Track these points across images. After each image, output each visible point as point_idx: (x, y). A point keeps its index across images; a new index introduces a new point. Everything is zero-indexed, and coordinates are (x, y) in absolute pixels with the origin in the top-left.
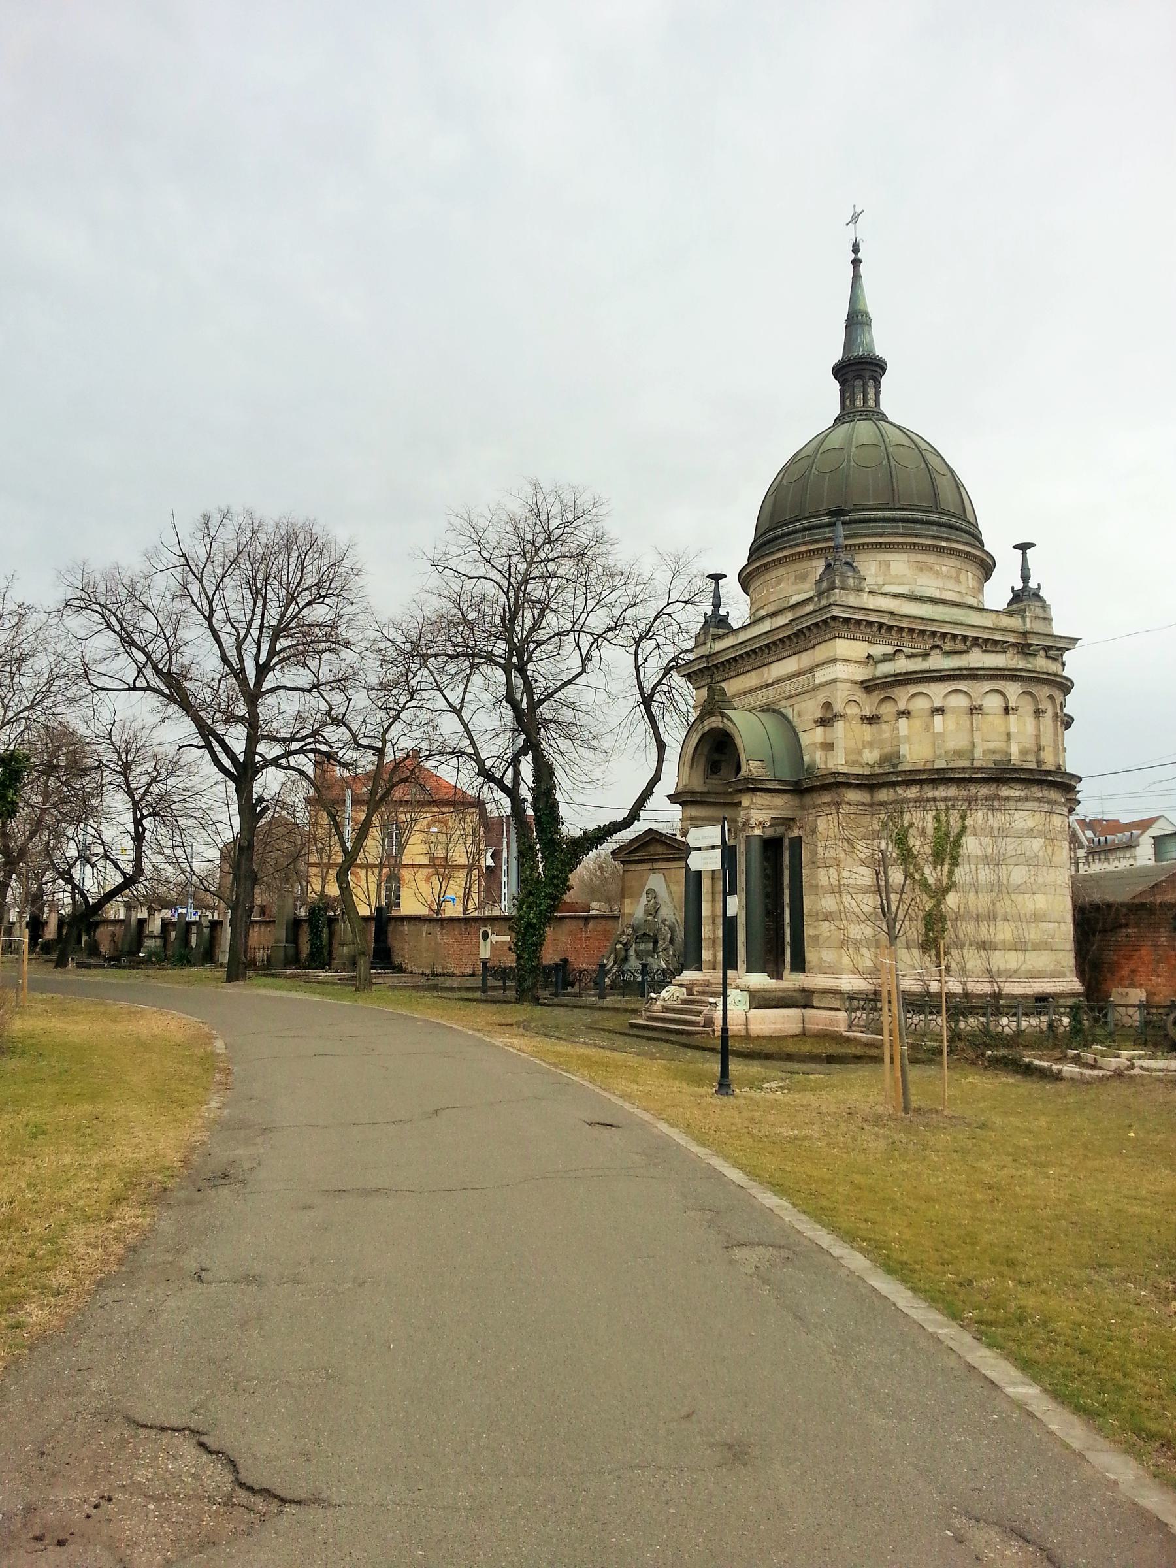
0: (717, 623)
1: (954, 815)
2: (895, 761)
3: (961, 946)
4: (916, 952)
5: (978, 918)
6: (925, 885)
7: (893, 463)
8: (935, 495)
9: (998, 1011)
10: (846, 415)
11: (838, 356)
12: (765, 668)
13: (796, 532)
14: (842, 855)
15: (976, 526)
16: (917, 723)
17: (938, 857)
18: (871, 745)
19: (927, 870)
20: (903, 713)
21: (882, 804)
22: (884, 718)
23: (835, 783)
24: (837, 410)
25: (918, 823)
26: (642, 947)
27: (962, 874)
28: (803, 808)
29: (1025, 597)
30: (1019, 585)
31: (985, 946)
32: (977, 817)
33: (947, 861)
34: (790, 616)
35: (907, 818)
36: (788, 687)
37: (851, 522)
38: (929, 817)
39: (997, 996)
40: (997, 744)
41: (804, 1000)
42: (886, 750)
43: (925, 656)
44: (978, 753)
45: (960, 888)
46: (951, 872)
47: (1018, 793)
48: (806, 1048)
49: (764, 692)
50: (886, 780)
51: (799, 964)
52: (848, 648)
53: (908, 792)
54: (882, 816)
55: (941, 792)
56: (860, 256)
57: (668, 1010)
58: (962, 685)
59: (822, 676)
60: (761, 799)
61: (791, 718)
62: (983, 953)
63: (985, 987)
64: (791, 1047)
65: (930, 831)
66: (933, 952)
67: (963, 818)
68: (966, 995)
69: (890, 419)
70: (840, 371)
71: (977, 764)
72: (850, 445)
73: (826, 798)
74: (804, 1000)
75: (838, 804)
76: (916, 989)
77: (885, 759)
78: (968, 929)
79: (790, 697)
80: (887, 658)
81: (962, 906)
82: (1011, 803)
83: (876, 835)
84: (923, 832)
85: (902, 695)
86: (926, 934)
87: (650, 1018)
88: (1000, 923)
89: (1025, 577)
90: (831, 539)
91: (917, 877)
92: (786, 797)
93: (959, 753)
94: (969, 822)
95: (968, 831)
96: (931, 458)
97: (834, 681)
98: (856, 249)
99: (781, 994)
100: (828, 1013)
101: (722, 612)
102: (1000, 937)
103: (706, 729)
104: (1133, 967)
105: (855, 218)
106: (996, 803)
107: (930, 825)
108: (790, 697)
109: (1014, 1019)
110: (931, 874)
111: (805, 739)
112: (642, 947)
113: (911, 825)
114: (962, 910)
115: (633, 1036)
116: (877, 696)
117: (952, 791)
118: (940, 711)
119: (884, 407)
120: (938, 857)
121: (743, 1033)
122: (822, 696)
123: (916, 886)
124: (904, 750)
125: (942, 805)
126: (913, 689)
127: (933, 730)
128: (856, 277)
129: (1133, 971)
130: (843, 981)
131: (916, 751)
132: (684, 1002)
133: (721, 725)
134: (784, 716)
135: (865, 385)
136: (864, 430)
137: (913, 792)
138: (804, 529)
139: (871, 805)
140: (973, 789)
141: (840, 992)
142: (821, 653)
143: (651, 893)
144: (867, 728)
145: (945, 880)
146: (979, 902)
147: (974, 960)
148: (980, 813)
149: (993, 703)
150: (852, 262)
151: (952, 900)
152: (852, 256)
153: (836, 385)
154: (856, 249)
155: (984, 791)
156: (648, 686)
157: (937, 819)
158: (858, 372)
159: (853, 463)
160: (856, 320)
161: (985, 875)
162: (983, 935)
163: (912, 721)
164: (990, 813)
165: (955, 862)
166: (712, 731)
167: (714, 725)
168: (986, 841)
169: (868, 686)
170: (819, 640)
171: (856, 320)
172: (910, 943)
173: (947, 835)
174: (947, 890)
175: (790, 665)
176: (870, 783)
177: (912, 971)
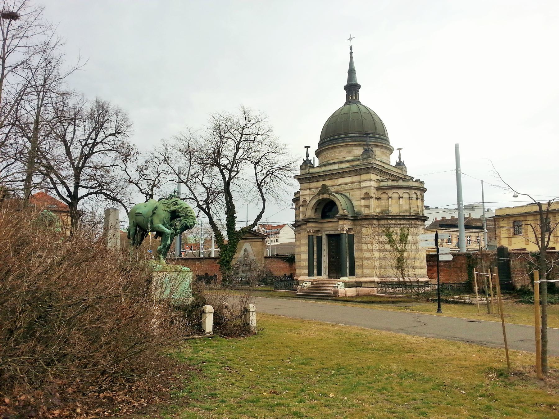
1: (406, 229)
3: (408, 267)
4: (395, 269)
5: (412, 259)
6: (397, 249)
8: (376, 129)
9: (419, 287)
10: (348, 102)
16: (394, 201)
17: (401, 241)
18: (378, 207)
19: (398, 245)
21: (382, 225)
23: (369, 218)
24: (345, 101)
26: (244, 269)
27: (408, 246)
28: (355, 225)
29: (400, 164)
30: (398, 161)
31: (414, 267)
34: (347, 165)
35: (391, 230)
36: (347, 187)
38: (399, 229)
39: (418, 282)
40: (415, 208)
41: (358, 284)
42: (383, 209)
43: (397, 181)
46: (405, 246)
48: (359, 299)
49: (336, 187)
50: (384, 217)
51: (352, 273)
52: (373, 176)
55: (402, 222)
57: (309, 289)
58: (408, 191)
59: (363, 184)
60: (346, 222)
63: (414, 280)
64: (354, 299)
65: (399, 233)
68: (410, 282)
69: (362, 103)
70: (346, 88)
71: (412, 214)
73: (366, 222)
74: (358, 284)
76: (396, 280)
77: (382, 211)
79: (348, 190)
83: (380, 234)
84: (397, 234)
85: (390, 193)
87: (303, 292)
89: (400, 158)
90: (365, 141)
91: (395, 247)
92: (351, 221)
93: (406, 211)
96: (374, 116)
97: (371, 186)
98: (351, 49)
102: (417, 265)
105: (351, 39)
107: (399, 232)
108: (348, 190)
110: (399, 247)
111: (355, 204)
112: (244, 269)
113: (393, 231)
116: (380, 192)
117: (405, 222)
118: (391, 198)
119: (360, 100)
120: (401, 241)
122: (364, 191)
124: (390, 209)
126: (394, 191)
127: (397, 204)
128: (351, 58)
131: (394, 209)
132: (312, 287)
133: (328, 197)
134: (344, 195)
136: (354, 108)
137: (393, 222)
138: (350, 137)
141: (374, 282)
142: (364, 177)
143: (245, 250)
146: (412, 255)
147: (411, 272)
149: (406, 195)
151: (405, 254)
153: (344, 92)
154: (351, 49)
155: (413, 222)
156: (259, 181)
157: (401, 230)
158: (352, 88)
160: (351, 72)
161: (413, 247)
162: (413, 265)
165: (406, 243)
166: (324, 200)
167: (325, 197)
168: (414, 237)
169: (378, 189)
171: (351, 72)
175: (348, 180)
176: (379, 218)
177: (393, 276)
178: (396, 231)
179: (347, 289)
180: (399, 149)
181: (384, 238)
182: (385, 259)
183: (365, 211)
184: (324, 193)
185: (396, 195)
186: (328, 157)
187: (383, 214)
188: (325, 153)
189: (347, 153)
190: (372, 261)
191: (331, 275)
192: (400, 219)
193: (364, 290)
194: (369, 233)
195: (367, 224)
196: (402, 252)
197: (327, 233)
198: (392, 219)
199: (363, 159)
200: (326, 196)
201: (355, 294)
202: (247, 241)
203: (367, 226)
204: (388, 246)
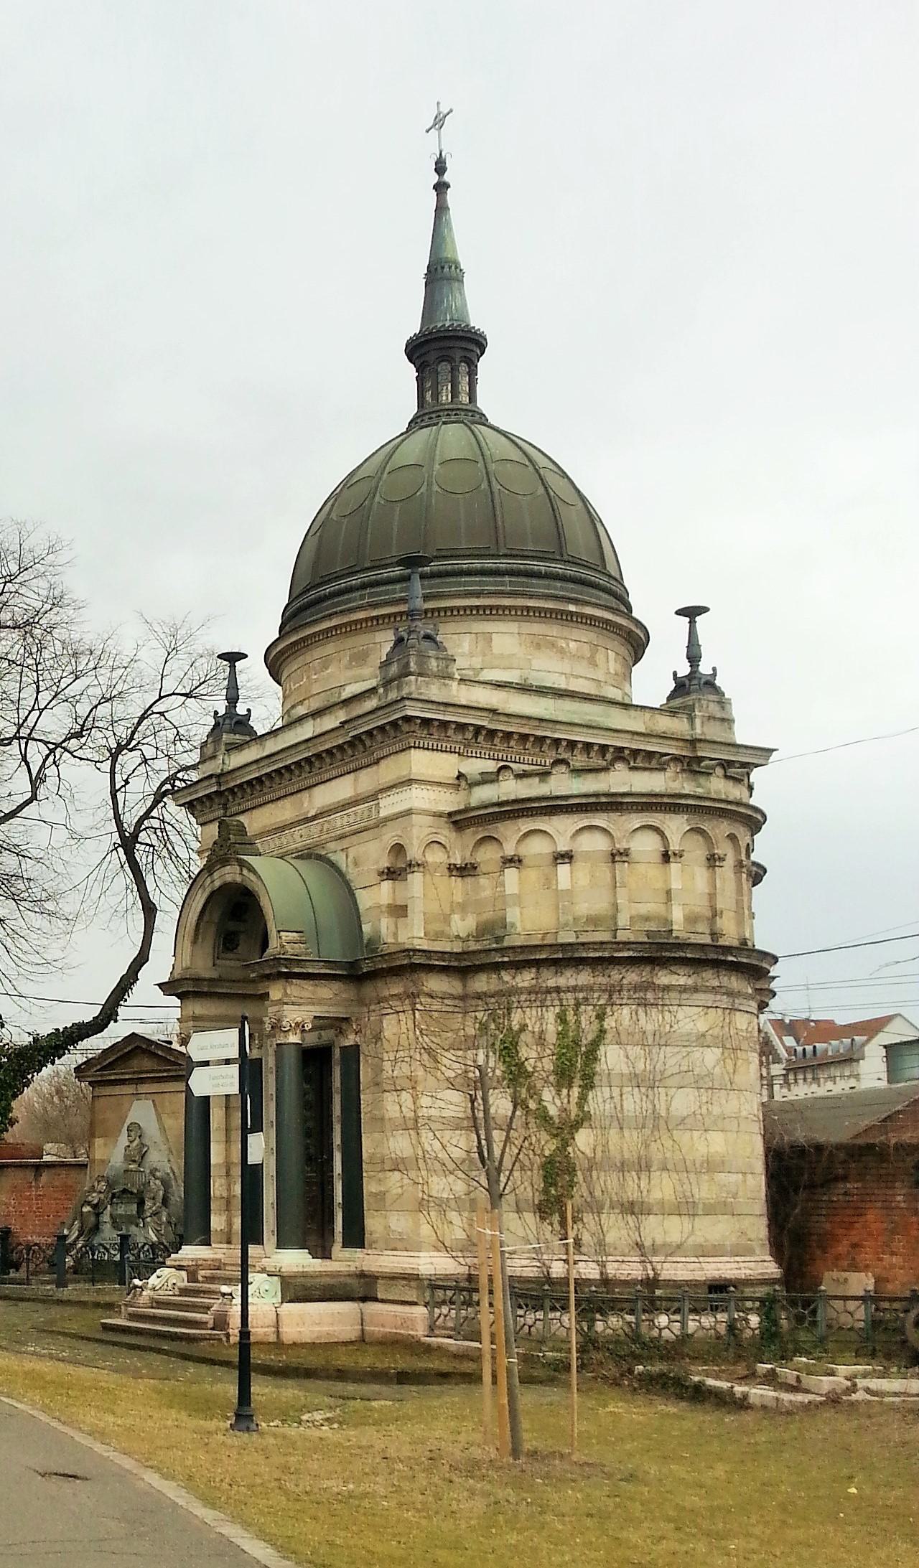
1: (588, 1013)
2: (499, 933)
4: (530, 1218)
5: (623, 1167)
6: (544, 1118)
7: (496, 487)
9: (653, 1306)
10: (426, 416)
12: (305, 794)
14: (420, 1073)
15: (619, 581)
16: (532, 875)
17: (563, 1076)
18: (463, 908)
19: (547, 1095)
20: (511, 861)
21: (479, 996)
22: (483, 868)
23: (409, 966)
24: (414, 409)
25: (534, 1026)
26: (121, 1210)
27: (598, 1101)
28: (361, 1002)
29: (693, 688)
30: (684, 669)
31: (632, 1209)
32: (622, 1017)
33: (577, 1082)
34: (342, 715)
36: (340, 822)
37: (433, 575)
38: (550, 1015)
40: (651, 907)
41: (362, 1289)
43: (544, 775)
44: (623, 921)
47: (682, 980)
48: (366, 1361)
50: (484, 961)
51: (355, 1237)
52: (421, 762)
53: (518, 978)
54: (480, 1015)
55: (568, 978)
56: (447, 177)
57: (160, 1304)
58: (600, 820)
60: (297, 989)
61: (343, 868)
62: (630, 1219)
63: (632, 1270)
65: (551, 1037)
66: (556, 1218)
67: (601, 1017)
68: (605, 1281)
69: (492, 421)
70: (418, 350)
71: (622, 936)
73: (396, 987)
74: (362, 1289)
76: (532, 1272)
77: (484, 930)
78: (607, 1183)
80: (487, 779)
81: (599, 1149)
82: (673, 994)
83: (470, 1043)
84: (541, 1039)
85: (510, 834)
86: (546, 1191)
87: (133, 1317)
88: (656, 1175)
89: (694, 657)
93: (594, 921)
94: (609, 1023)
95: (609, 1036)
97: (408, 813)
98: (440, 168)
99: (329, 1280)
101: (241, 709)
102: (656, 1195)
103: (217, 884)
104: (855, 1239)
105: (439, 121)
106: (650, 995)
107: (552, 1028)
109: (678, 1317)
110: (552, 1101)
112: (121, 1210)
113: (523, 1028)
114: (599, 1154)
115: (108, 1342)
116: (472, 835)
117: (584, 977)
118: (567, 857)
119: (483, 403)
120: (563, 1076)
121: (272, 1338)
122: (389, 836)
123: (531, 1120)
124: (513, 915)
125: (569, 998)
126: (526, 825)
127: (557, 886)
129: (854, 1246)
130: (421, 1261)
131: (530, 919)
132: (184, 1292)
133: (239, 879)
134: (333, 865)
135: (454, 371)
136: (453, 437)
137: (525, 979)
138: (363, 586)
139: (463, 998)
140: (616, 974)
142: (388, 771)
143: (135, 1129)
144: (457, 883)
146: (624, 1144)
147: (617, 1230)
148: (626, 1010)
149: (646, 845)
150: (436, 187)
151: (584, 1140)
152: (435, 178)
154: (440, 168)
155: (632, 976)
156: (130, 819)
157: (562, 1018)
158: (444, 351)
160: (441, 274)
161: (633, 1103)
162: (631, 1193)
164: (641, 1010)
165: (589, 1083)
166: (226, 887)
167: (229, 878)
169: (459, 821)
171: (441, 274)
172: (522, 1205)
173: (576, 1043)
174: (576, 1125)
175: (341, 789)
176: (462, 966)
177: (524, 1246)
178: (538, 1023)
179: (288, 1307)
185: (598, 843)
187: (486, 944)
189: (349, 667)
192: (557, 964)
193: (385, 1317)
196: (566, 1129)
198: (518, 966)
199: (387, 683)
201: (348, 1331)
202: (144, 1088)
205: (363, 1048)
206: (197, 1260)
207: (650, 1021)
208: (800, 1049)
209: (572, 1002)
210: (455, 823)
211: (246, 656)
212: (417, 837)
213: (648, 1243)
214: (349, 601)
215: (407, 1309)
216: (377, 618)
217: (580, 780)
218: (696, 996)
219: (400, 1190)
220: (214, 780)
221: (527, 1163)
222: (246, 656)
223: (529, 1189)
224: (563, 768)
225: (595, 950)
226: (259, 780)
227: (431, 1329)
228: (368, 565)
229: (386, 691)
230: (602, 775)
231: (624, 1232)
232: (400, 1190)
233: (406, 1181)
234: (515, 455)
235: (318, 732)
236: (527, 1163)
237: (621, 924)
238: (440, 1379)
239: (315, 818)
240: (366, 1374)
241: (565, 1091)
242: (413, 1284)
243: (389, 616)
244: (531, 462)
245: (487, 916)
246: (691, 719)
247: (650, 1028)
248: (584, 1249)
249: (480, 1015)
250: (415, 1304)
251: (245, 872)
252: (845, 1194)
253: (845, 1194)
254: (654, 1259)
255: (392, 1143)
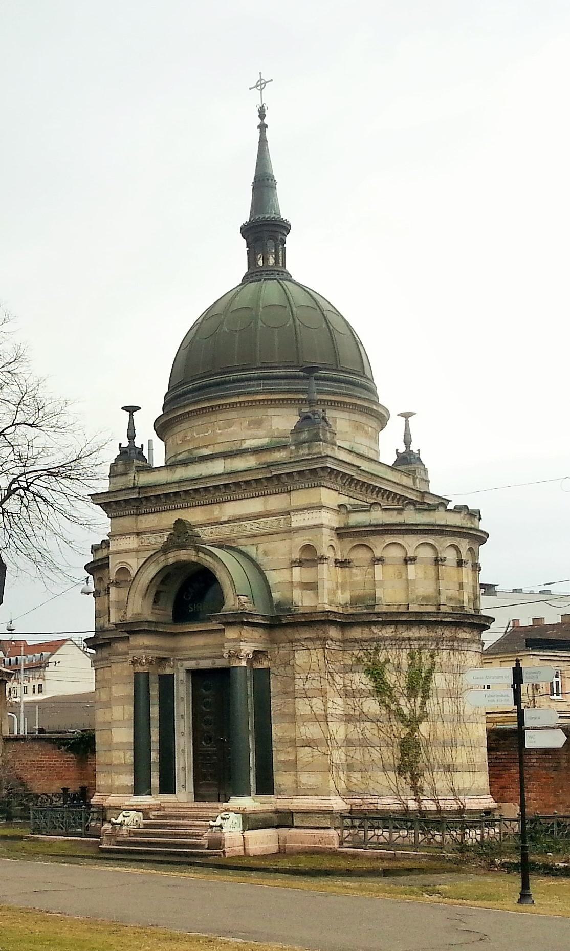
0: (130, 456)
1: (426, 654)
2: (370, 603)
4: (392, 775)
5: (444, 745)
6: (400, 714)
7: (298, 322)
10: (254, 274)
11: (245, 217)
12: (216, 507)
13: (250, 379)
16: (391, 570)
17: (412, 690)
18: (343, 586)
19: (402, 701)
20: (378, 560)
22: (355, 563)
23: (316, 621)
24: (244, 269)
27: (431, 706)
28: (273, 641)
30: (402, 449)
31: (449, 769)
32: (443, 656)
33: (420, 694)
36: (250, 527)
38: (404, 654)
39: (461, 811)
40: (453, 592)
42: (357, 593)
44: (443, 600)
45: (430, 717)
47: (468, 636)
48: (285, 864)
50: (361, 618)
52: (328, 496)
53: (384, 631)
54: (356, 652)
55: (414, 633)
56: (266, 121)
57: (136, 834)
58: (431, 540)
59: (298, 520)
61: (254, 556)
62: (448, 774)
63: (450, 805)
66: (408, 775)
67: (432, 656)
70: (246, 231)
71: (443, 609)
72: (258, 305)
74: (283, 820)
75: (325, 639)
76: (396, 807)
77: (355, 601)
78: (436, 753)
80: (357, 510)
81: (432, 734)
82: (465, 644)
83: (347, 669)
84: (398, 668)
85: (379, 545)
86: (402, 759)
87: (118, 843)
88: (459, 748)
89: (407, 441)
91: (393, 707)
93: (426, 599)
94: (437, 659)
97: (321, 526)
98: (262, 114)
99: (261, 816)
100: (315, 831)
102: (459, 761)
103: (171, 561)
104: (503, 784)
105: (261, 85)
106: (456, 644)
107: (405, 662)
114: (432, 737)
115: (101, 858)
116: (348, 543)
117: (423, 632)
118: (380, 560)
119: (289, 267)
121: (242, 853)
122: (301, 540)
123: (393, 716)
124: (379, 593)
126: (389, 539)
128: (263, 142)
129: (503, 788)
130: (332, 802)
131: (390, 594)
132: (147, 826)
133: (194, 559)
136: (270, 290)
137: (388, 632)
138: (259, 378)
139: (344, 641)
141: (331, 812)
142: (299, 498)
145: (418, 712)
146: (444, 730)
147: (442, 782)
148: (445, 652)
149: (426, 554)
150: (259, 127)
151: (424, 728)
152: (259, 121)
154: (262, 114)
155: (447, 633)
157: (411, 656)
158: (265, 233)
159: (260, 323)
160: (263, 184)
162: (448, 760)
163: (385, 568)
165: (426, 696)
166: (180, 566)
167: (184, 558)
168: (449, 676)
169: (342, 533)
170: (329, 485)
171: (263, 184)
174: (420, 721)
175: (254, 506)
176: (345, 622)
177: (387, 793)
178: (396, 661)
179: (248, 833)
180: (406, 416)
181: (361, 681)
182: (364, 743)
183: (303, 601)
184: (181, 547)
185: (395, 553)
186: (193, 439)
188: (185, 425)
190: (324, 749)
191: (203, 791)
192: (409, 624)
194: (314, 666)
195: (310, 639)
196: (412, 723)
197: (192, 665)
198: (385, 624)
199: (299, 444)
200: (186, 555)
201: (273, 847)
203: (309, 645)
204: (372, 706)
205: (273, 670)
206: (149, 805)
207: (455, 659)
208: (7, 659)
209: (417, 647)
210: (338, 534)
211: (140, 408)
212: (326, 543)
213: (456, 789)
214: (248, 386)
215: (322, 831)
216: (271, 400)
217: (420, 515)
218: (474, 645)
219: (310, 759)
220: (137, 490)
221: (390, 742)
222: (140, 408)
223: (391, 757)
224: (412, 507)
225: (434, 617)
226: (176, 494)
227: (341, 843)
228: (260, 365)
229: (297, 448)
230: (432, 513)
231: (445, 782)
232: (310, 759)
233: (316, 753)
234: (312, 304)
235: (228, 470)
236: (390, 742)
237: (442, 602)
238: (408, 873)
239: (225, 522)
240: (364, 871)
241: (413, 700)
242: (328, 816)
243: (279, 400)
244: (320, 313)
245: (359, 592)
246: (414, 479)
247: (455, 663)
248: (424, 793)
249: (356, 652)
250: (328, 828)
251: (201, 555)
252: (496, 758)
253: (496, 758)
254: (461, 797)
255: (303, 730)
